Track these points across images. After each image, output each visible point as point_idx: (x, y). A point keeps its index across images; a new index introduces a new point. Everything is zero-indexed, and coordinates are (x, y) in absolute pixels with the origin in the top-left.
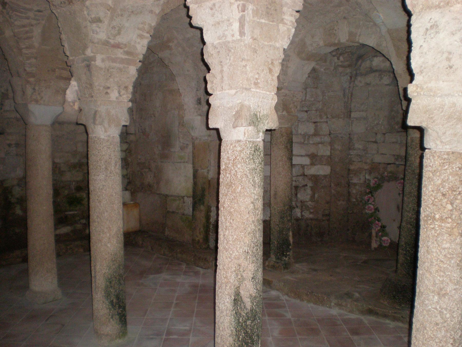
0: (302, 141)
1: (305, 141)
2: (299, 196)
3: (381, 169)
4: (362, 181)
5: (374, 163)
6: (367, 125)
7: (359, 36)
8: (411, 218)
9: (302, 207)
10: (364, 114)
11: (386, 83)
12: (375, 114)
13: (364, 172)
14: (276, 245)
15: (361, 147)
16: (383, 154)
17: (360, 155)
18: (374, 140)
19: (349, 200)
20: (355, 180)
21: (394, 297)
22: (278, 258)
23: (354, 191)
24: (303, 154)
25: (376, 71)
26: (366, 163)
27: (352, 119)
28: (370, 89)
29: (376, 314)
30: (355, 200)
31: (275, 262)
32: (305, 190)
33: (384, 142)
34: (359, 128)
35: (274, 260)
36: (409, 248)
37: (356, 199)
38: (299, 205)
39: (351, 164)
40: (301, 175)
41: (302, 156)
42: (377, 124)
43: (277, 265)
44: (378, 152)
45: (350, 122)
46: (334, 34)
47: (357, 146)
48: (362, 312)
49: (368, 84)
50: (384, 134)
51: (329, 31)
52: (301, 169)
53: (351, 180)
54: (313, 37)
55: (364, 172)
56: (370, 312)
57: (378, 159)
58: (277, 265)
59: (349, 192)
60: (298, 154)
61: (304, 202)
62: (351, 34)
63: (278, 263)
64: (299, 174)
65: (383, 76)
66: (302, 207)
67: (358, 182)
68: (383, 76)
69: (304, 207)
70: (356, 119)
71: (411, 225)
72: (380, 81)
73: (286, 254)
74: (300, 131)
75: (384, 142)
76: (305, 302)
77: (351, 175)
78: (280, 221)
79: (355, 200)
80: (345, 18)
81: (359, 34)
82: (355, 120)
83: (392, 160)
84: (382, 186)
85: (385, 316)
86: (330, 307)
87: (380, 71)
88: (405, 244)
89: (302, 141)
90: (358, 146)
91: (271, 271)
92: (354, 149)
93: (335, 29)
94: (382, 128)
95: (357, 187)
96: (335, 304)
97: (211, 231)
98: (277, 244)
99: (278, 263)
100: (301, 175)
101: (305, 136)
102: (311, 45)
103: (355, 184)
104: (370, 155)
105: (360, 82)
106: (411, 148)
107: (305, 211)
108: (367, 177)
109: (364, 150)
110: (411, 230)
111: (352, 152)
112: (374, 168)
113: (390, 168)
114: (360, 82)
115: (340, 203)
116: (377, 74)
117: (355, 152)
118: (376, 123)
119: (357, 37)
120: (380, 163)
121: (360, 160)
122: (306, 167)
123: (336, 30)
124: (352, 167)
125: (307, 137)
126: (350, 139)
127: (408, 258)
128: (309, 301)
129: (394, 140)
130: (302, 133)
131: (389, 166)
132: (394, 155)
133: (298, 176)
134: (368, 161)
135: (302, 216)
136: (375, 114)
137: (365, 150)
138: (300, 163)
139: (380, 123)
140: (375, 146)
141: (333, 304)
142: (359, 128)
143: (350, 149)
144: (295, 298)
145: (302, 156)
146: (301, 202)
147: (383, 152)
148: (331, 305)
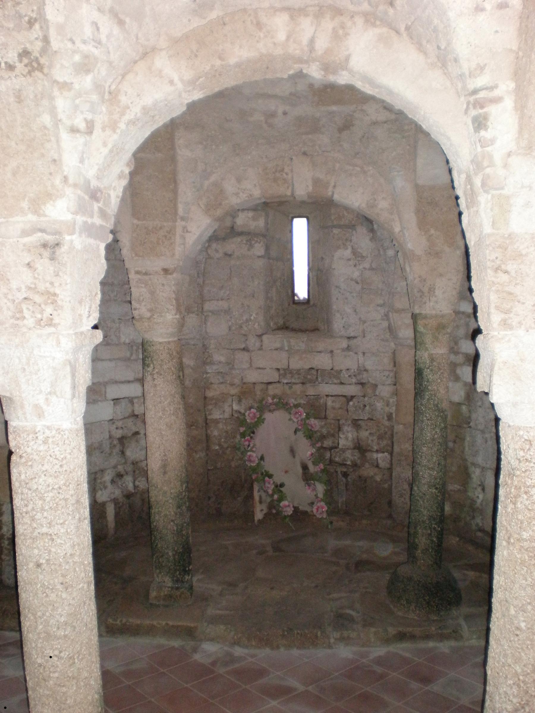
0: (128, 354)
1: (132, 355)
2: (128, 453)
3: (258, 393)
4: (227, 415)
5: (244, 383)
6: (230, 323)
7: (334, 187)
8: (436, 479)
9: (134, 472)
10: (224, 305)
11: (260, 254)
12: (242, 304)
13: (230, 400)
14: (171, 558)
15: (223, 359)
16: (260, 368)
17: (221, 372)
18: (243, 346)
19: (208, 448)
20: (216, 415)
21: (428, 603)
22: (177, 581)
23: (216, 433)
24: (131, 379)
25: (241, 234)
26: (232, 385)
27: (205, 314)
28: (233, 262)
29: (412, 637)
30: (217, 448)
31: (172, 588)
32: (137, 441)
33: (260, 349)
34: (217, 328)
35: (170, 584)
36: (436, 524)
37: (220, 445)
38: (130, 468)
39: (209, 389)
40: (128, 417)
41: (129, 382)
42: (247, 321)
43: (178, 593)
44: (251, 366)
45: (203, 317)
46: (285, 180)
47: (217, 357)
48: (387, 641)
49: (227, 255)
50: (260, 336)
51: (274, 173)
52: (129, 405)
53: (210, 414)
54: (239, 180)
55: (230, 400)
56: (401, 637)
57: (252, 377)
58: (178, 593)
59: (207, 436)
60: (123, 380)
61: (137, 462)
62: (316, 182)
63: (177, 588)
64: (127, 415)
65: (253, 242)
66: (134, 472)
67: (221, 417)
68: (253, 242)
69: (137, 472)
70: (213, 312)
71: (436, 488)
72: (249, 250)
73: (189, 569)
74: (123, 339)
75: (260, 349)
76: (282, 649)
77: (210, 407)
78: (176, 514)
79: (217, 448)
80: (305, 154)
81: (332, 184)
82: (210, 314)
83: (275, 377)
84: (264, 419)
85: (427, 637)
86: (330, 647)
87: (249, 233)
88: (429, 519)
89: (128, 354)
90: (219, 357)
91: (167, 606)
92: (212, 363)
93: (286, 171)
94: (256, 326)
95: (221, 426)
96: (336, 639)
97: (6, 552)
98: (174, 555)
99: (177, 588)
100: (128, 417)
101: (132, 346)
102: (237, 194)
103: (217, 422)
104: (238, 372)
105: (217, 251)
106: (431, 370)
107: (139, 479)
108: (236, 407)
109: (228, 364)
110: (438, 496)
111: (209, 369)
112: (246, 391)
113: (272, 390)
114: (217, 251)
115: (198, 456)
116: (244, 238)
117: (215, 367)
118: (244, 318)
119: (330, 189)
120: (254, 383)
121: (221, 380)
122: (135, 401)
123: (287, 174)
124: (210, 394)
125: (135, 348)
126: (205, 347)
127: (435, 539)
128: (289, 647)
129: (278, 345)
130: (127, 341)
131: (270, 387)
132: (278, 370)
133: (125, 418)
134: (237, 381)
135: (135, 487)
136: (242, 304)
137: (230, 364)
138: (127, 396)
139: (252, 318)
140: (245, 356)
141: (332, 640)
142: (217, 328)
143: (205, 363)
144: (259, 648)
145: (129, 382)
146: (133, 464)
147: (261, 366)
148: (330, 643)
